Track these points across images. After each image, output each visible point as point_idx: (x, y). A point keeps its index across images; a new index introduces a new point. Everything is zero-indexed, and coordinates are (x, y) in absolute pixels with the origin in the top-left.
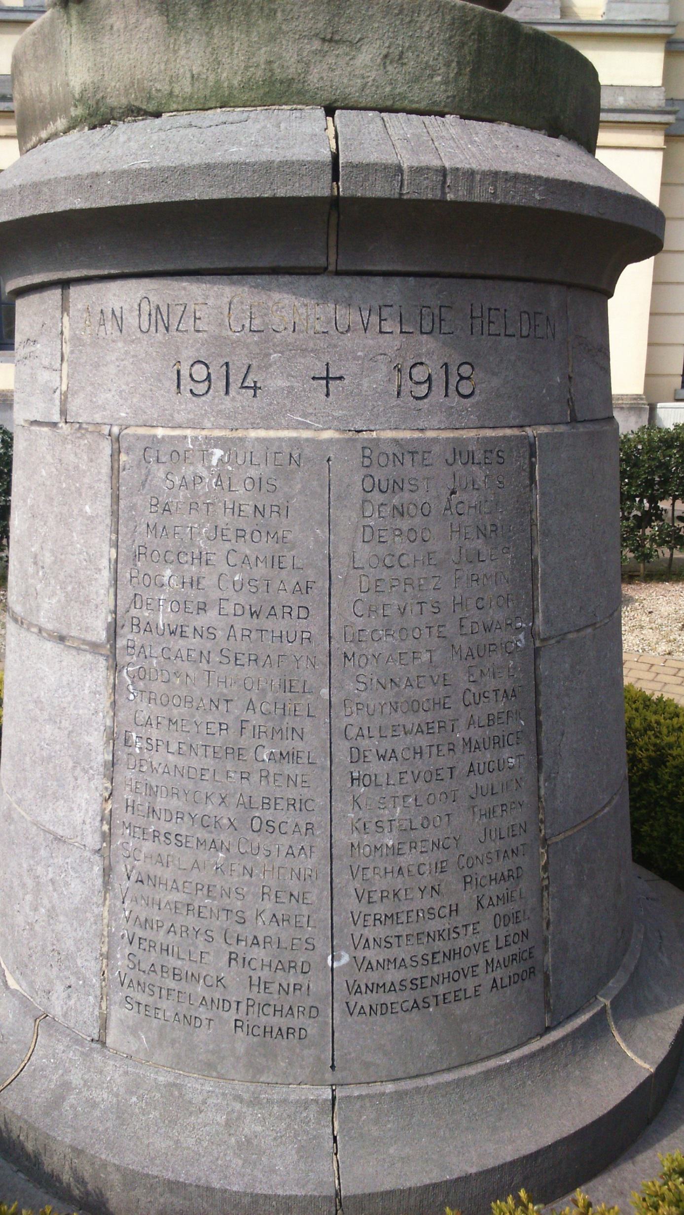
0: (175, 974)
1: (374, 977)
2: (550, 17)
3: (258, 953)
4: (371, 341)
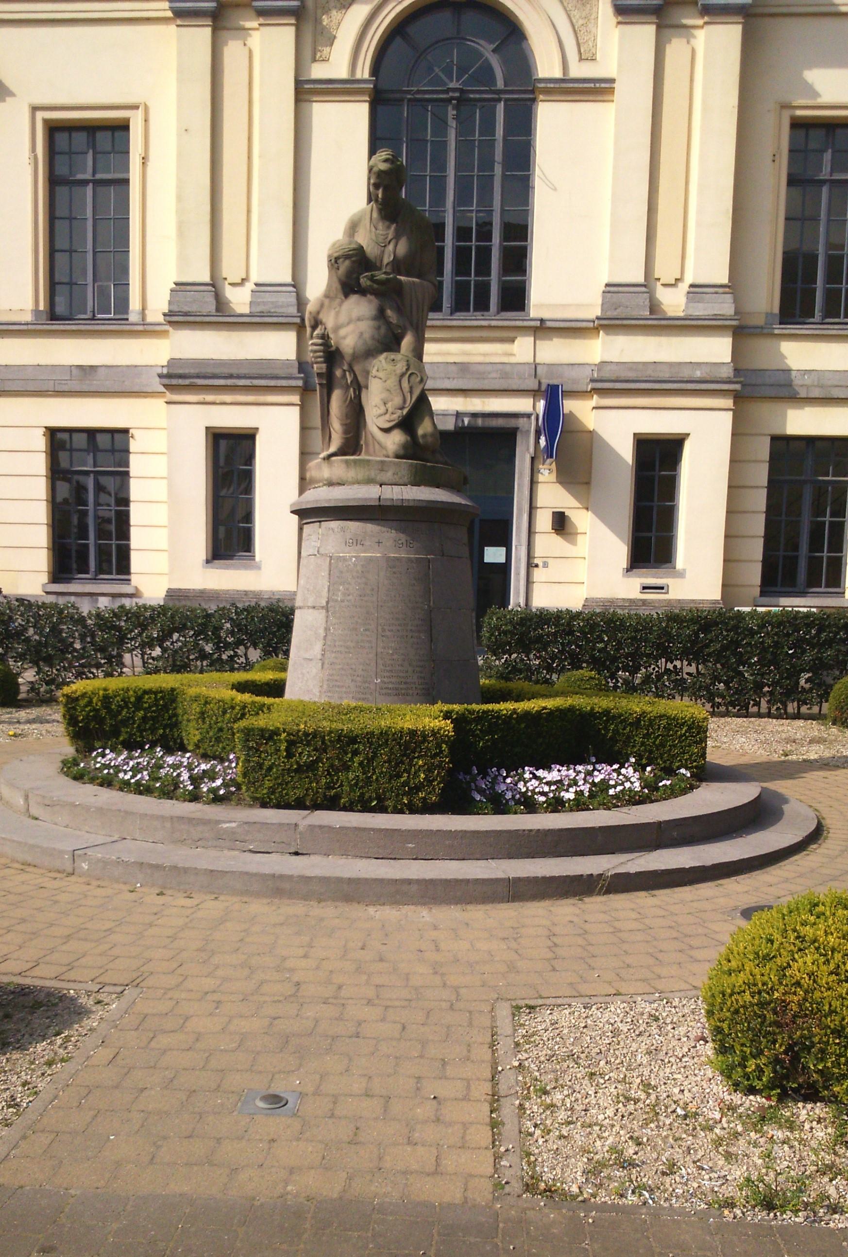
0: (338, 687)
1: (386, 686)
2: (642, 313)
3: (358, 679)
4: (388, 534)
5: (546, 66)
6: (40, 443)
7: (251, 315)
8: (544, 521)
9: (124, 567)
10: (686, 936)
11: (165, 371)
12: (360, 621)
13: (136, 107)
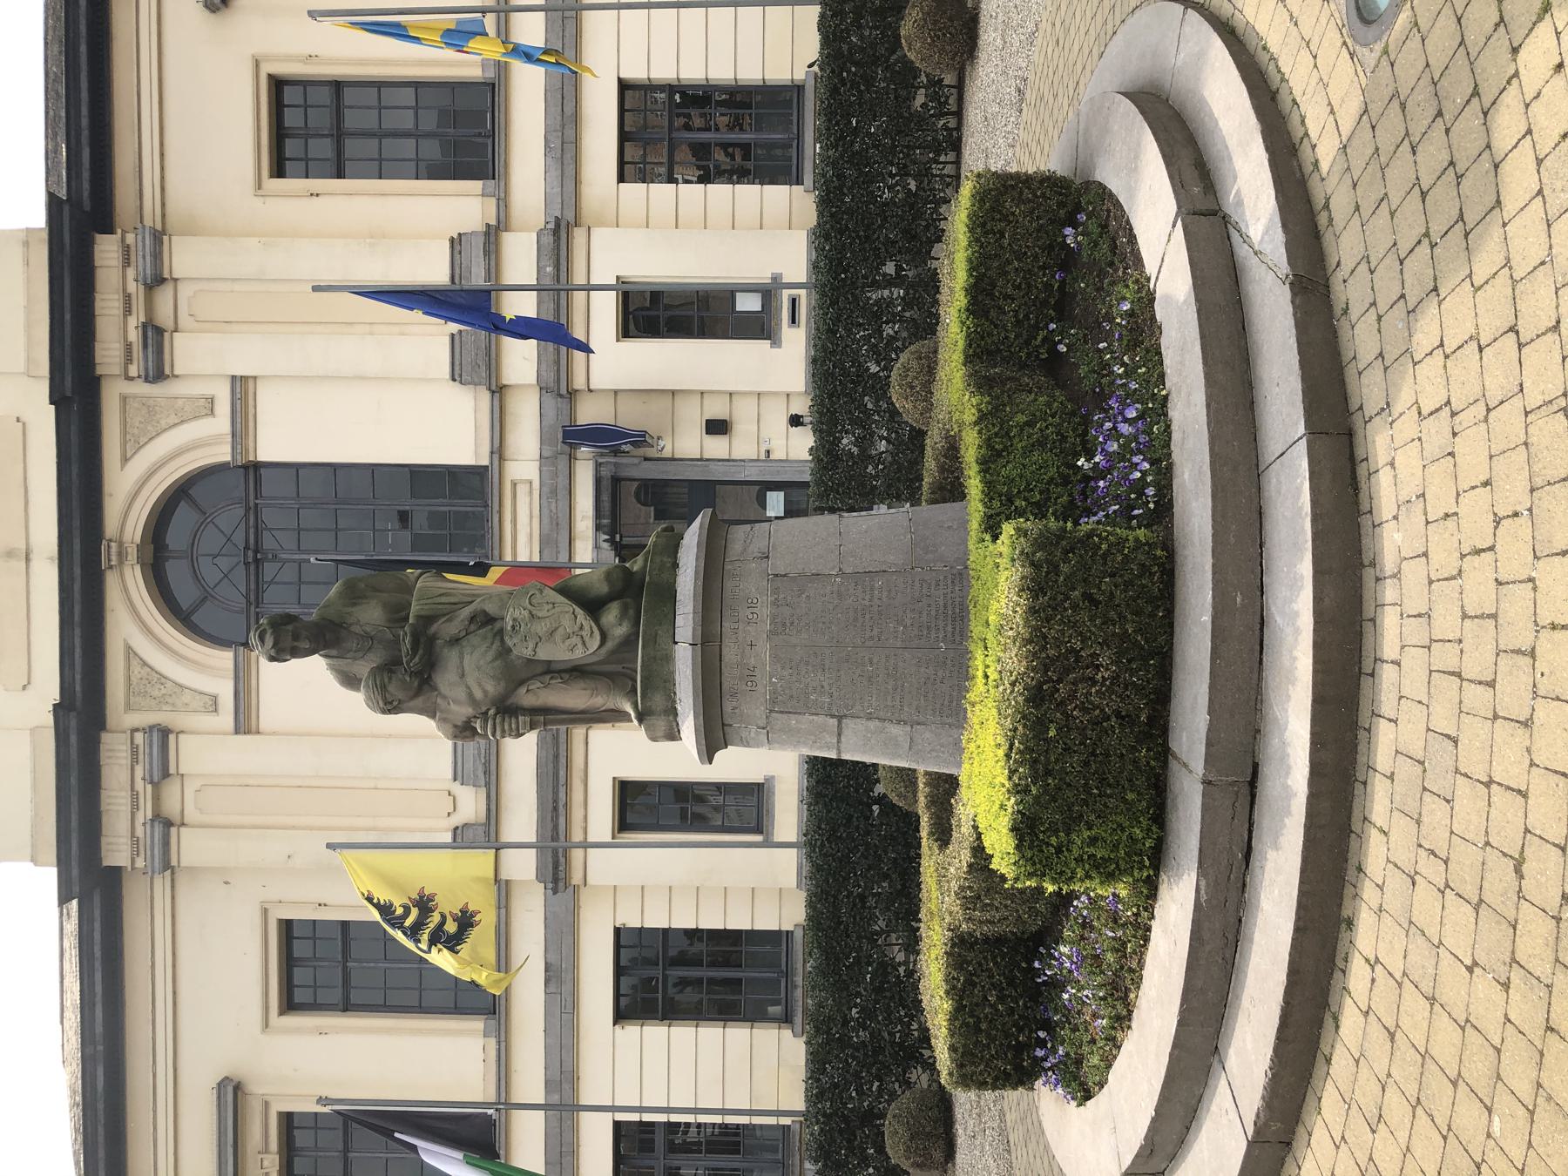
5: (223, 454)
6: (632, 1031)
7: (487, 785)
8: (716, 447)
11: (550, 885)
12: (858, 672)
13: (265, 911)
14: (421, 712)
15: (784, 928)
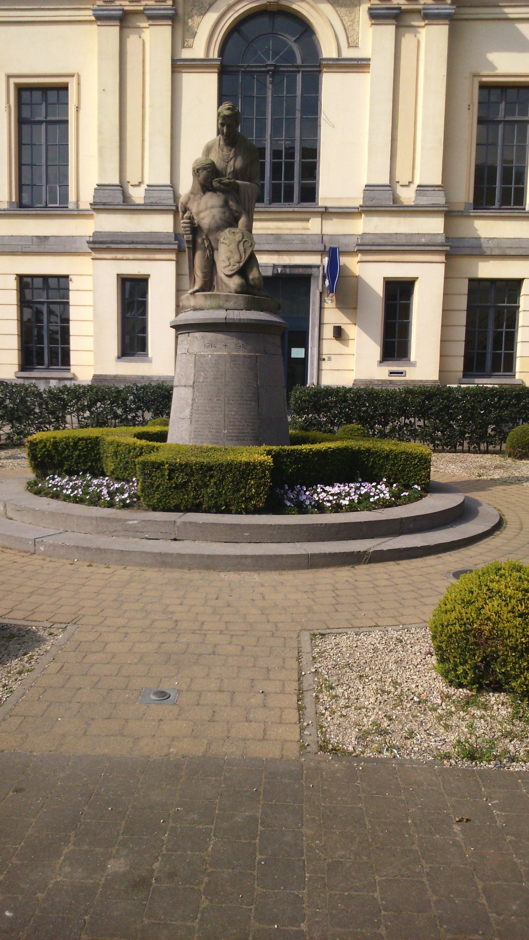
1: (231, 434)
2: (388, 203)
3: (213, 430)
5: (328, 51)
6: (13, 284)
8: (328, 332)
9: (66, 361)
10: (413, 591)
11: (91, 239)
13: (73, 76)
14: (193, 187)
15: (72, 368)
